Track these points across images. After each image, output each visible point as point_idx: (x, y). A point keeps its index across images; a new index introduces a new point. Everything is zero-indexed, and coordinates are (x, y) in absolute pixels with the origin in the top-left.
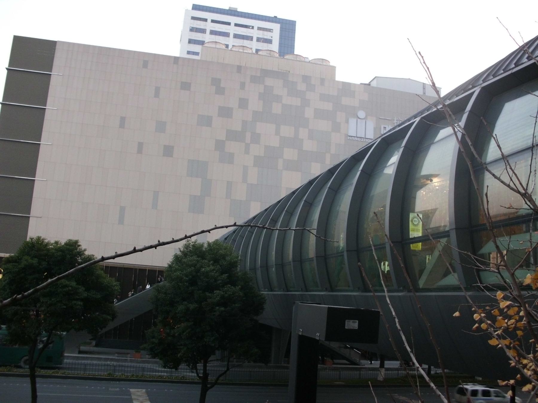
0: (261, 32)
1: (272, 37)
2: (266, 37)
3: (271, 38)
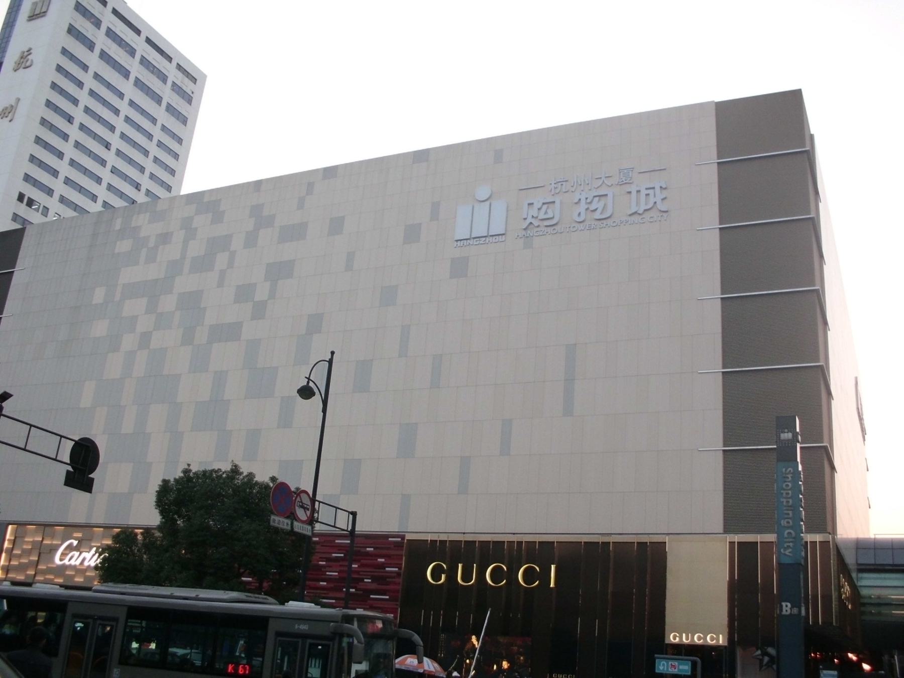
0: (175, 78)
1: (193, 93)
2: (184, 88)
3: (190, 93)
